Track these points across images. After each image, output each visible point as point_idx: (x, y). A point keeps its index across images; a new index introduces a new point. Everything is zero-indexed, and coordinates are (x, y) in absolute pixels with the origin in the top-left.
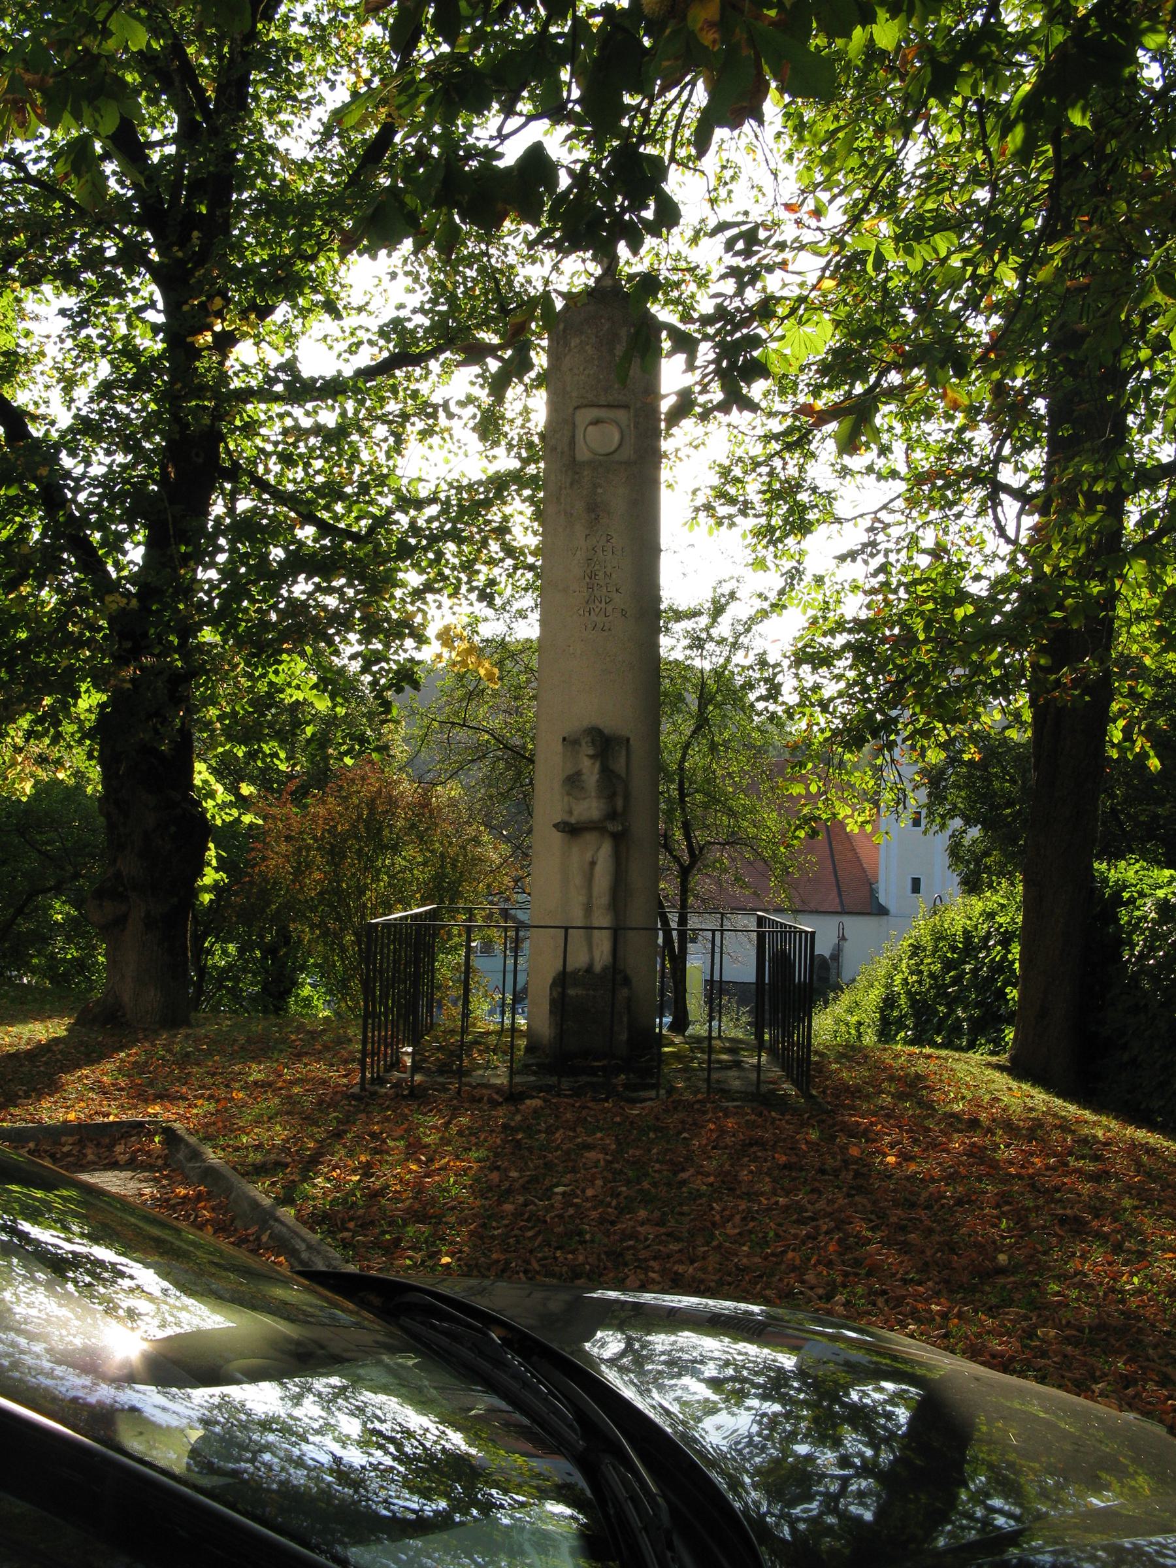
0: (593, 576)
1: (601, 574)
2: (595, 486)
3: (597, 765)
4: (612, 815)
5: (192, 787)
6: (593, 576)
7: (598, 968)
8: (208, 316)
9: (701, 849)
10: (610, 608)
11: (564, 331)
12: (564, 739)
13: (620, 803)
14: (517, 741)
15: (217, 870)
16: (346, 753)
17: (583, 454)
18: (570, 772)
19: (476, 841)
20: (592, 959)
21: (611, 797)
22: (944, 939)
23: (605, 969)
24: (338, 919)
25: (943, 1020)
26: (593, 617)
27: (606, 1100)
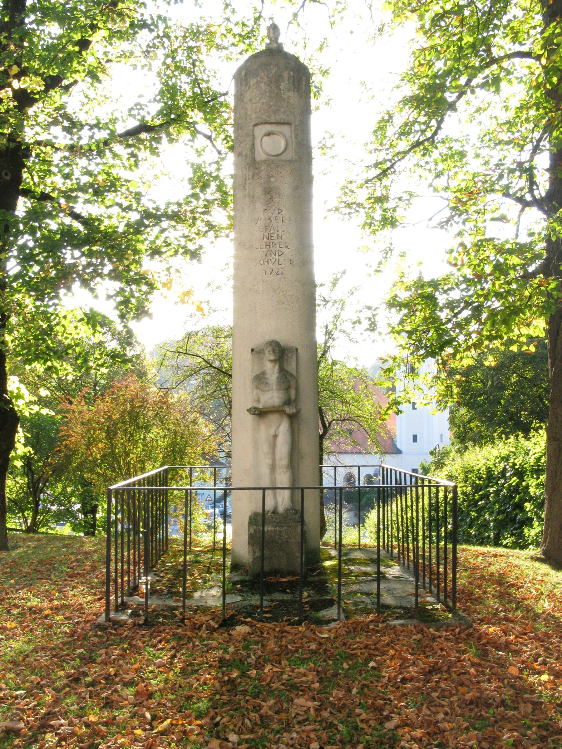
0: (269, 237)
1: (275, 236)
2: (269, 177)
3: (277, 367)
4: (288, 402)
5: (6, 391)
6: (269, 237)
7: (281, 509)
8: (8, 78)
9: (330, 424)
10: (282, 259)
11: (245, 76)
12: (252, 350)
13: (293, 393)
14: (217, 364)
15: (25, 445)
16: (102, 366)
17: (260, 156)
18: (257, 373)
19: (194, 422)
20: (276, 503)
21: (288, 389)
22: (472, 472)
23: (287, 511)
24: (114, 471)
25: (473, 521)
26: (271, 265)
27: (299, 623)
